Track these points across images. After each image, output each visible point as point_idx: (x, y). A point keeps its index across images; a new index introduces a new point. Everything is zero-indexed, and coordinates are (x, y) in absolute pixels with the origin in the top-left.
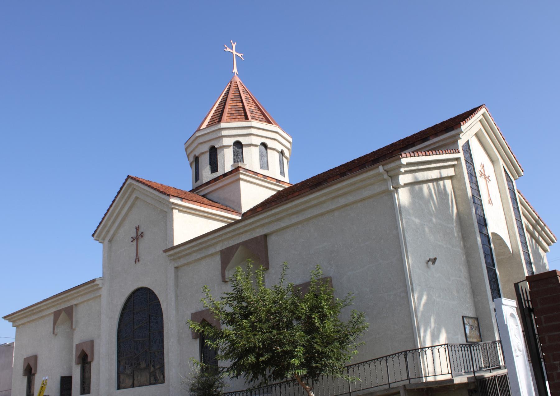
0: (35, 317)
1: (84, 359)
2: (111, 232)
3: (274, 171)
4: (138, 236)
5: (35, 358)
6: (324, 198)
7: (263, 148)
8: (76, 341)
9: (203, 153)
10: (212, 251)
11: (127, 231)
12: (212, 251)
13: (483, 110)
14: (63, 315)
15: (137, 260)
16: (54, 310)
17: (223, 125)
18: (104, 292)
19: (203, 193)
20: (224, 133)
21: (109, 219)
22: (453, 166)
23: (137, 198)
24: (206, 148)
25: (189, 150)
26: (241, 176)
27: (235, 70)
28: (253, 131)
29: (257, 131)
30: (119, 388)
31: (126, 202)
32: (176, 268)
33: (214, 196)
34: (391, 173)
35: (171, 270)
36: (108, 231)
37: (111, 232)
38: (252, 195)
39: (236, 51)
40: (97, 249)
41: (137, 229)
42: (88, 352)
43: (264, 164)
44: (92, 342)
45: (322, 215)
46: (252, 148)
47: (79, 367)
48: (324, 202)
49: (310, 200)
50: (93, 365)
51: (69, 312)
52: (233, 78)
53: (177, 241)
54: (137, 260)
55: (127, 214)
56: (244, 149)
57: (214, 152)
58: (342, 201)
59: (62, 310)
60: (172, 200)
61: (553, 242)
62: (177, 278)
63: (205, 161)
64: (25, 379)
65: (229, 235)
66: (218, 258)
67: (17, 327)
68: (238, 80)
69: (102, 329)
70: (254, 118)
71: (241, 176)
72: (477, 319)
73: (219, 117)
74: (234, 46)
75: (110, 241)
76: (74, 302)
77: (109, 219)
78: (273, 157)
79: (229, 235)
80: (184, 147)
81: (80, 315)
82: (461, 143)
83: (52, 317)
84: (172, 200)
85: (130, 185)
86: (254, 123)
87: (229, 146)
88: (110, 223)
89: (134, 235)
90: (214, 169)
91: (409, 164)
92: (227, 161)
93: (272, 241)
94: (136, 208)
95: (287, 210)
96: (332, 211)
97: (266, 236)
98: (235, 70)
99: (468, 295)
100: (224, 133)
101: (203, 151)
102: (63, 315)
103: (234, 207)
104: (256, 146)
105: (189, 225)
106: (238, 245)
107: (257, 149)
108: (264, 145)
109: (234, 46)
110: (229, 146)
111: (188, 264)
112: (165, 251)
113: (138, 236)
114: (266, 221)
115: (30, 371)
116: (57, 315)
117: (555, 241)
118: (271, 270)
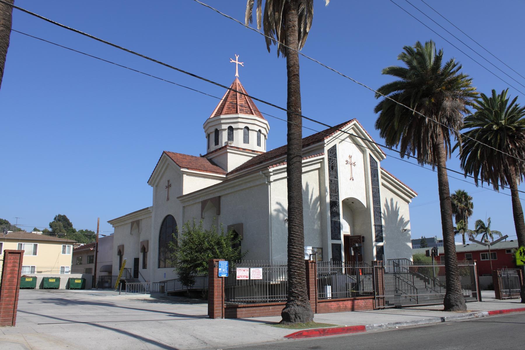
0: (123, 223)
1: (144, 250)
2: (157, 181)
3: (253, 145)
4: (169, 186)
5: (123, 246)
6: (241, 182)
7: (246, 130)
8: (141, 241)
9: (211, 133)
10: (198, 201)
11: (163, 183)
12: (198, 201)
13: (355, 122)
14: (135, 225)
15: (168, 199)
16: (131, 221)
17: (222, 116)
18: (153, 215)
19: (209, 158)
20: (222, 121)
21: (155, 174)
22: (320, 162)
23: (168, 164)
24: (213, 130)
25: (206, 128)
26: (228, 150)
27: (237, 75)
28: (240, 120)
29: (244, 119)
30: (159, 267)
31: (163, 165)
32: (184, 207)
33: (215, 160)
34: (266, 175)
35: (182, 208)
36: (155, 181)
37: (157, 181)
38: (234, 161)
39: (238, 61)
40: (150, 189)
41: (169, 181)
42: (146, 247)
43: (246, 140)
44: (148, 241)
45: (241, 190)
46: (239, 130)
47: (142, 254)
48: (242, 184)
49: (236, 182)
50: (148, 253)
51: (138, 223)
52: (235, 80)
53: (185, 193)
54: (168, 199)
55: (164, 172)
56: (234, 131)
57: (217, 133)
58: (249, 185)
59: (134, 221)
60: (182, 170)
61: (414, 196)
62: (184, 212)
63: (213, 137)
64: (119, 257)
65: (204, 194)
66: (200, 205)
67: (115, 227)
68: (238, 81)
69: (152, 234)
70: (242, 111)
71: (228, 150)
72: (322, 249)
73: (220, 112)
74: (237, 58)
75: (157, 186)
76: (140, 218)
77: (155, 174)
78: (253, 136)
79: (204, 194)
80: (203, 127)
81: (143, 224)
82: (327, 148)
83: (130, 225)
84: (182, 170)
85: (165, 156)
86: (240, 115)
87: (225, 130)
88: (156, 176)
89: (167, 185)
90: (217, 143)
91: (274, 171)
92: (224, 137)
93: (222, 199)
94: (167, 170)
95: (227, 185)
96: (245, 189)
97: (220, 197)
98: (237, 75)
99: (317, 236)
100: (222, 121)
101: (211, 131)
102: (135, 225)
103: (225, 167)
104: (242, 129)
105: (192, 184)
106: (208, 199)
107: (242, 131)
108: (247, 128)
109: (237, 58)
110: (225, 130)
111: (189, 205)
112: (178, 198)
113: (169, 186)
114: (219, 189)
115: (120, 253)
116: (132, 223)
117: (416, 195)
118: (221, 215)
